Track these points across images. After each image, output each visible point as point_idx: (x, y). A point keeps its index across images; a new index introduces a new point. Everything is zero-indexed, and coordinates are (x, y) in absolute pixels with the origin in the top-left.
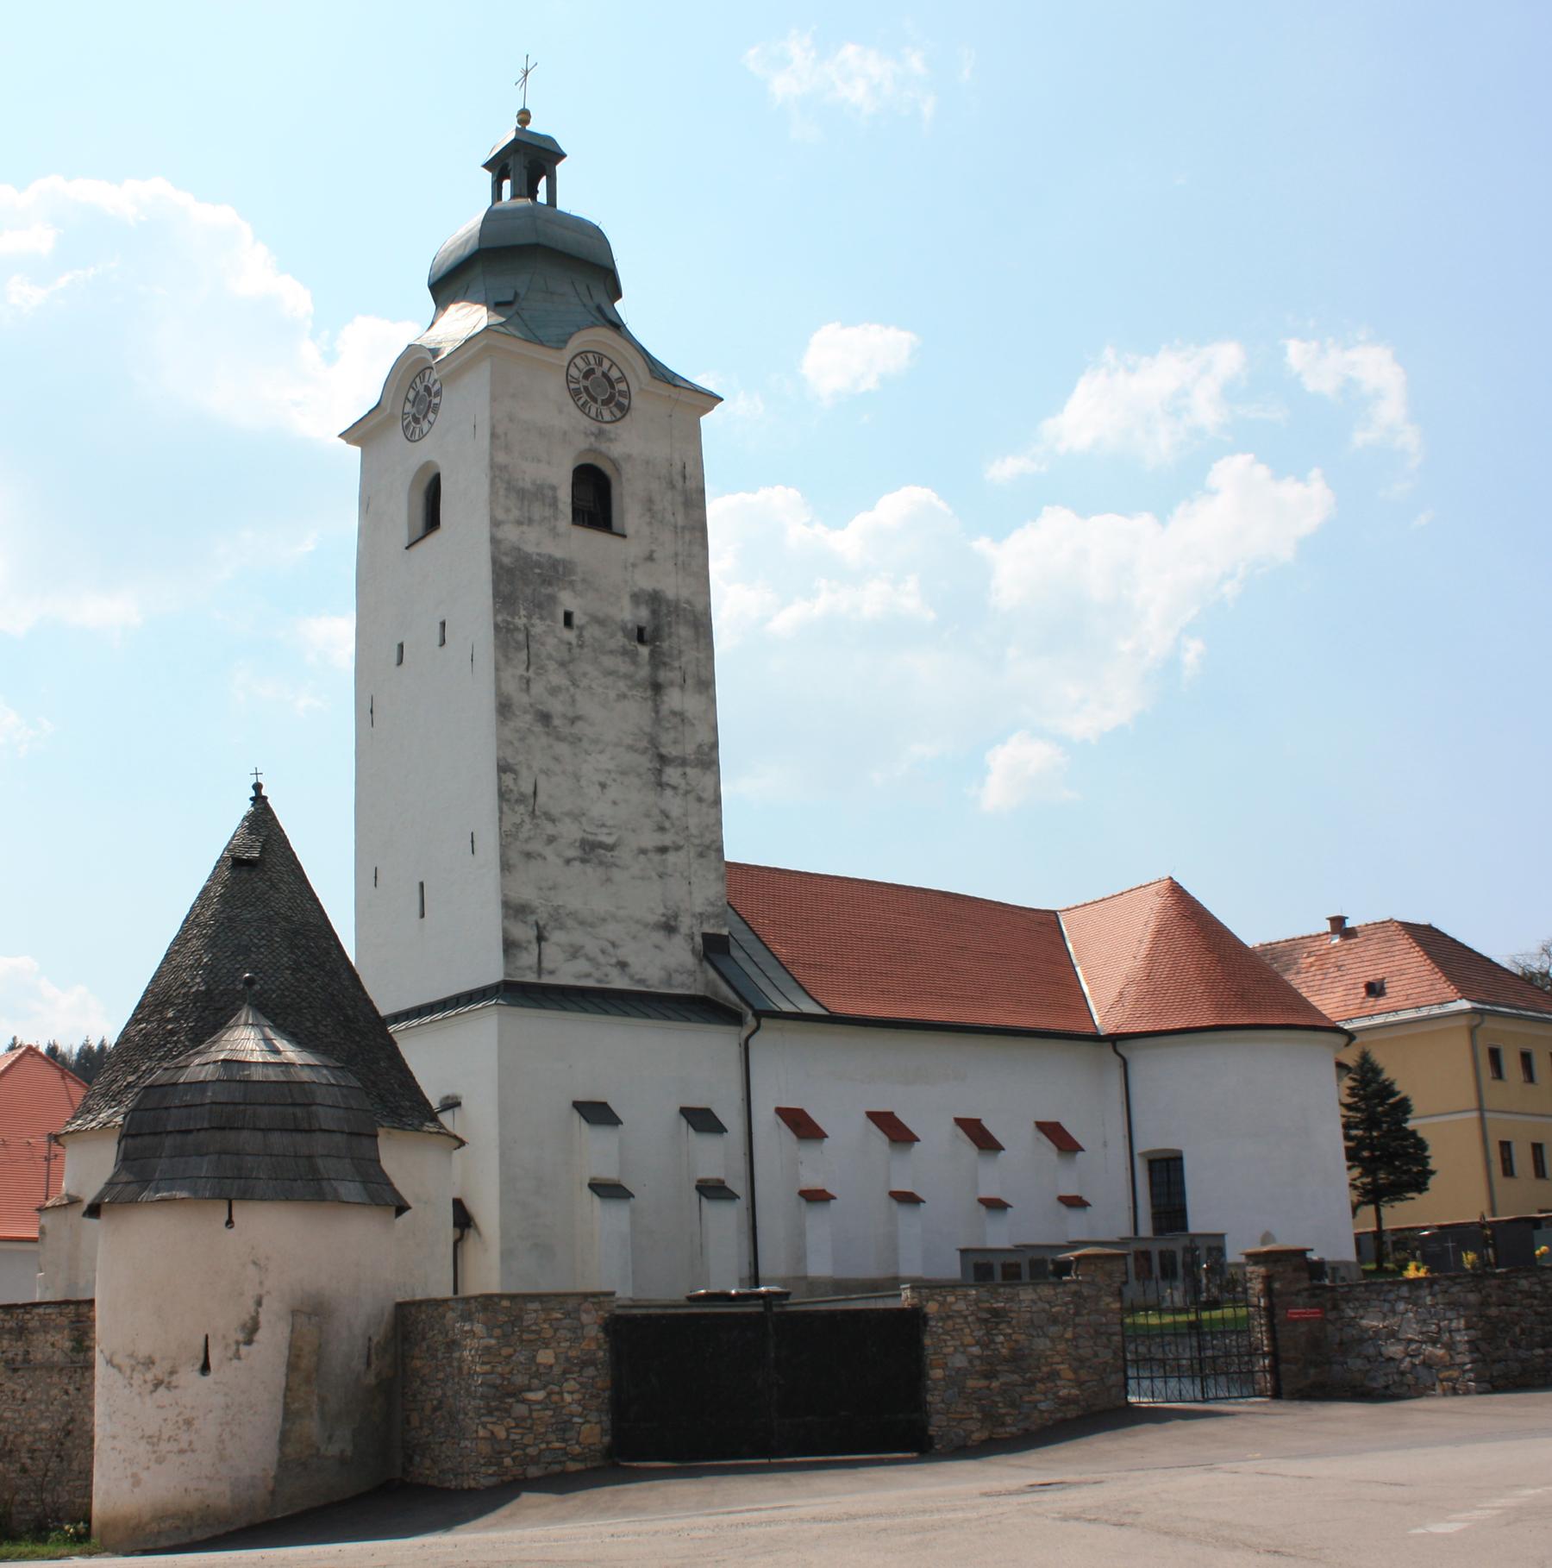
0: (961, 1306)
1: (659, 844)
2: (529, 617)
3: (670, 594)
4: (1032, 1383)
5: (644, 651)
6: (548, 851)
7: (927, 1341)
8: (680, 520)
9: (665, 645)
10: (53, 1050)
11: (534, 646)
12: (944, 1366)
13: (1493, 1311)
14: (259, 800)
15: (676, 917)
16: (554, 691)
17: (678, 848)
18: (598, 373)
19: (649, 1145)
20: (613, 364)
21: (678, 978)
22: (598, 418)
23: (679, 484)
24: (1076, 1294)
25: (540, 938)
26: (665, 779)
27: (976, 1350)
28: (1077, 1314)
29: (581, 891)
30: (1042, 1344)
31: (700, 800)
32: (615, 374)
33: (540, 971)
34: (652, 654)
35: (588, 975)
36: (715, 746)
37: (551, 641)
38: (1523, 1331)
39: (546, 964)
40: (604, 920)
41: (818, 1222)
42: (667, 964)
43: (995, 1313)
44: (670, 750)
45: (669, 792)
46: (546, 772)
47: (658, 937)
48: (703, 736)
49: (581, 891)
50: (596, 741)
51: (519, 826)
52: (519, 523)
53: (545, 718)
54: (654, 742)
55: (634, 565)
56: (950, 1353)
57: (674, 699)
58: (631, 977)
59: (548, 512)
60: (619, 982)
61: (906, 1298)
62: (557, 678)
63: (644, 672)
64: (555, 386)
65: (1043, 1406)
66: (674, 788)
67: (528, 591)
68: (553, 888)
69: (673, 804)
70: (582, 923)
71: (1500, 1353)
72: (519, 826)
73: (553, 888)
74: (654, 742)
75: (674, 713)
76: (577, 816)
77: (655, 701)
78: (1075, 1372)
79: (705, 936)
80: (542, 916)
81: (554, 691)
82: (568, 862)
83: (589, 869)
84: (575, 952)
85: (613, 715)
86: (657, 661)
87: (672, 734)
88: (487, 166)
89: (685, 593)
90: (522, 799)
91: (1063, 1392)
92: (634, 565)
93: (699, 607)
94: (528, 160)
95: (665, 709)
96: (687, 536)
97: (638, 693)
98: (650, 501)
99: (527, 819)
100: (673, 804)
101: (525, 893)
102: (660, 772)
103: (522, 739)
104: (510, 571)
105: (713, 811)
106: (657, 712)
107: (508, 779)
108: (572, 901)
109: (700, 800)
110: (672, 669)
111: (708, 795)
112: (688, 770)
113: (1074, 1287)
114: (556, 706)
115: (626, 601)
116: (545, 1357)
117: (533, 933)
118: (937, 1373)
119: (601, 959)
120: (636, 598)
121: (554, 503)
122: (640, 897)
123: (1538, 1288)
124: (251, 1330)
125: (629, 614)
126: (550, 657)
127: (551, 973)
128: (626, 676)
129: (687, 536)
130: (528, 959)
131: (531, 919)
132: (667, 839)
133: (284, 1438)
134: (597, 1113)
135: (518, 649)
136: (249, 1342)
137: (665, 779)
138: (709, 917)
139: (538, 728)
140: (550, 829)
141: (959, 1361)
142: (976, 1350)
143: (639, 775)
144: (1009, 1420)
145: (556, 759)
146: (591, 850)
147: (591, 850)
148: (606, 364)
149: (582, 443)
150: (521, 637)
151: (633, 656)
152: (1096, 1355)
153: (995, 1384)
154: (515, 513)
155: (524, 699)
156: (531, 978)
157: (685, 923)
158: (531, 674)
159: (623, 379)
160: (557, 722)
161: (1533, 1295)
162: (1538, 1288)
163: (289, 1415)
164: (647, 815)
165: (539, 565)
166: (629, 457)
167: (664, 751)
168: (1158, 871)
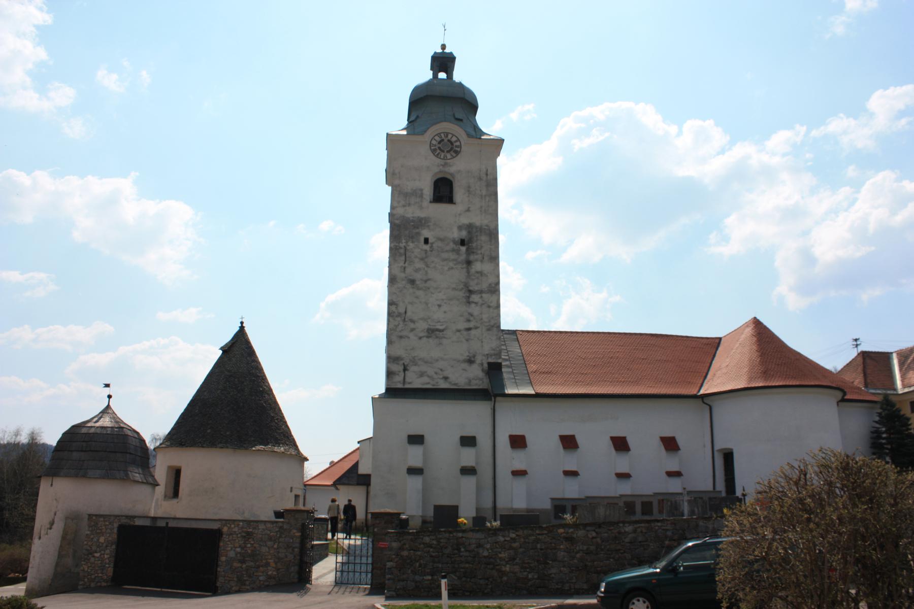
0: (236, 529)
1: (467, 327)
2: (407, 242)
3: (478, 224)
4: (258, 567)
5: (463, 249)
6: (411, 335)
7: (221, 544)
8: (484, 192)
9: (474, 245)
11: (408, 254)
12: (226, 556)
13: (405, 553)
14: (242, 328)
15: (474, 356)
16: (417, 270)
17: (476, 328)
18: (446, 140)
19: (444, 454)
20: (453, 135)
21: (474, 382)
22: (445, 158)
23: (485, 178)
24: (281, 527)
25: (405, 370)
26: (471, 300)
27: (238, 550)
28: (280, 537)
29: (427, 349)
30: (264, 549)
31: (489, 307)
32: (454, 139)
33: (404, 382)
34: (467, 250)
35: (428, 383)
36: (498, 283)
37: (417, 251)
38: (420, 566)
39: (407, 380)
40: (437, 360)
41: (520, 484)
42: (463, 376)
43: (248, 534)
44: (474, 286)
45: (473, 305)
46: (411, 303)
47: (465, 365)
48: (492, 280)
49: (427, 349)
50: (436, 288)
51: (397, 326)
52: (404, 206)
53: (412, 282)
54: (466, 285)
55: (460, 215)
56: (229, 550)
57: (477, 266)
58: (450, 383)
59: (418, 200)
60: (443, 385)
61: (215, 526)
62: (419, 265)
63: (463, 257)
64: (425, 149)
65: (261, 578)
66: (476, 303)
67: (407, 232)
68: (413, 349)
69: (475, 310)
70: (426, 362)
71: (405, 576)
72: (397, 326)
73: (413, 349)
74: (466, 285)
75: (477, 272)
76: (423, 319)
77: (467, 268)
78: (276, 564)
79: (489, 364)
80: (407, 362)
81: (417, 270)
82: (420, 338)
83: (431, 340)
84: (422, 374)
85: (446, 276)
86: (470, 252)
87: (476, 281)
89: (485, 222)
90: (399, 315)
91: (270, 573)
92: (460, 215)
93: (492, 227)
94: (443, 62)
95: (473, 271)
96: (487, 199)
97: (459, 266)
98: (469, 187)
99: (401, 323)
100: (475, 310)
101: (398, 352)
102: (469, 297)
103: (401, 291)
104: (399, 226)
105: (496, 311)
106: (468, 272)
107: (393, 308)
109: (489, 307)
110: (477, 254)
111: (494, 304)
112: (484, 295)
113: (280, 524)
114: (418, 276)
115: (455, 230)
116: (102, 540)
117: (401, 368)
118: (223, 559)
119: (435, 376)
120: (460, 228)
121: (421, 196)
122: (456, 349)
123: (435, 542)
124: (52, 523)
125: (456, 234)
126: (416, 257)
127: (410, 383)
128: (453, 260)
129: (487, 199)
131: (401, 362)
132: (471, 325)
133: (57, 565)
134: (416, 440)
135: (401, 255)
136: (51, 528)
137: (471, 300)
138: (491, 355)
139: (409, 286)
140: (412, 326)
141: (232, 554)
142: (238, 550)
143: (458, 300)
144: (247, 583)
145: (417, 297)
146: (432, 332)
147: (432, 332)
148: (450, 136)
149: (436, 170)
150: (402, 251)
151: (458, 252)
152: (286, 556)
153: (244, 566)
154: (403, 202)
155: (403, 275)
156: (400, 386)
157: (479, 359)
158: (406, 265)
159: (458, 140)
160: (418, 282)
161: (430, 546)
162: (435, 542)
163: (60, 556)
164: (461, 316)
165: (413, 221)
166: (459, 171)
167: (471, 288)
168: (748, 318)
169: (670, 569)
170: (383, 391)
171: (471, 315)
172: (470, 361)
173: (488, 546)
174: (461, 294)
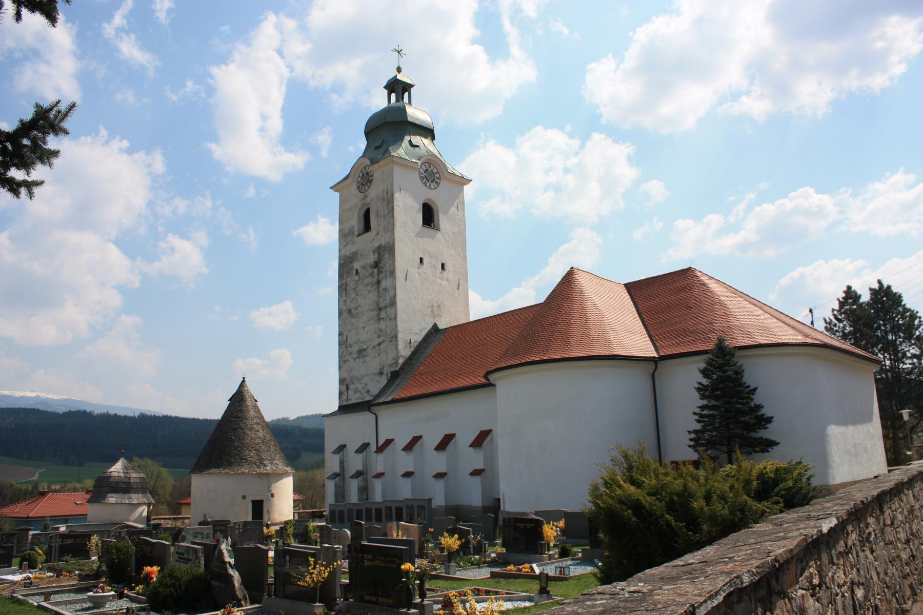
5: (376, 270)
10: (889, 287)
17: (384, 341)
25: (348, 389)
47: (378, 378)
57: (384, 284)
74: (378, 303)
84: (356, 391)
86: (379, 273)
88: (385, 87)
95: (381, 289)
108: (355, 373)
130: (345, 397)
169: (235, 567)
170: (337, 409)
171: (381, 330)
172: (381, 373)
173: (715, 376)
174: (375, 313)
